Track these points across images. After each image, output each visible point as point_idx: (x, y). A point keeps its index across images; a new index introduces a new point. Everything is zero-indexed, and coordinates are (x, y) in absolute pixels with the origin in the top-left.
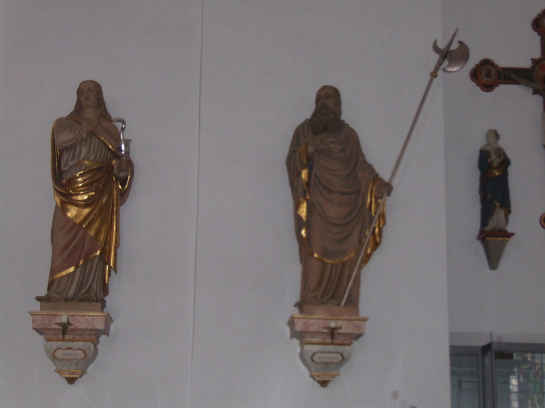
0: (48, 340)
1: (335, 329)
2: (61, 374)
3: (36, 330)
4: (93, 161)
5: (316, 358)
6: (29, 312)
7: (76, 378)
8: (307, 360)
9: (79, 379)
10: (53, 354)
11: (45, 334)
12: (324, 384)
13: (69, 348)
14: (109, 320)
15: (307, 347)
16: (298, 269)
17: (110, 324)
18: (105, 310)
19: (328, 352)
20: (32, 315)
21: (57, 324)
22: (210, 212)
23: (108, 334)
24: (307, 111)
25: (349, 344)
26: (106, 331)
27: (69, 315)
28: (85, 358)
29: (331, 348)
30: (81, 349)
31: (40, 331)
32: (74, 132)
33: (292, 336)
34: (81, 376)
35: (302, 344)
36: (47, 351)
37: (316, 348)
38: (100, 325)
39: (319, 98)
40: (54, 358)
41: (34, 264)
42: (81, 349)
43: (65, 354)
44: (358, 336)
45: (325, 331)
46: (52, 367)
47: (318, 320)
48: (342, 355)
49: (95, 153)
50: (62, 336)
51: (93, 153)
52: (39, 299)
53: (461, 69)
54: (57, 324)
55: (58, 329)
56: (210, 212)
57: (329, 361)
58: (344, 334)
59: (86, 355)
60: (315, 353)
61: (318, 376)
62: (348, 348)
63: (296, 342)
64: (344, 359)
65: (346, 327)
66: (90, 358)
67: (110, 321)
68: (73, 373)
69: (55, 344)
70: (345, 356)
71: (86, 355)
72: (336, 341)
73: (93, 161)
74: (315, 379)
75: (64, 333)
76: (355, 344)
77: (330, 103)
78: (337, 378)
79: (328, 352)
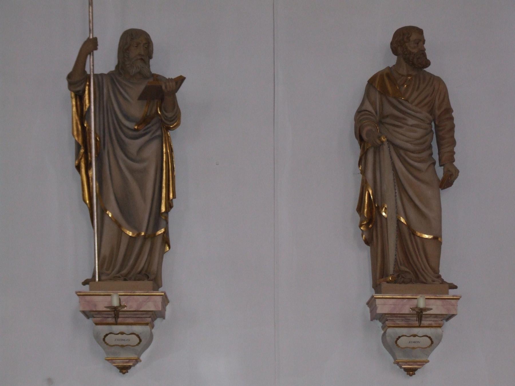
0: (97, 324)
3: (84, 312)
6: (76, 293)
7: (129, 367)
8: (392, 346)
9: (132, 368)
10: (104, 339)
13: (122, 333)
14: (165, 300)
15: (390, 331)
22: (264, 191)
23: (164, 317)
25: (440, 327)
27: (426, 299)
28: (139, 343)
30: (427, 336)
31: (87, 314)
32: (405, 119)
34: (134, 365)
36: (96, 336)
41: (66, 240)
42: (427, 336)
43: (119, 340)
44: (449, 317)
45: (108, 310)
49: (145, 132)
51: (145, 130)
53: (93, 55)
56: (264, 191)
58: (436, 316)
59: (140, 340)
60: (107, 335)
61: (406, 363)
62: (439, 330)
64: (433, 343)
65: (436, 307)
66: (143, 342)
69: (104, 329)
71: (140, 340)
72: (120, 320)
75: (420, 319)
78: (427, 365)
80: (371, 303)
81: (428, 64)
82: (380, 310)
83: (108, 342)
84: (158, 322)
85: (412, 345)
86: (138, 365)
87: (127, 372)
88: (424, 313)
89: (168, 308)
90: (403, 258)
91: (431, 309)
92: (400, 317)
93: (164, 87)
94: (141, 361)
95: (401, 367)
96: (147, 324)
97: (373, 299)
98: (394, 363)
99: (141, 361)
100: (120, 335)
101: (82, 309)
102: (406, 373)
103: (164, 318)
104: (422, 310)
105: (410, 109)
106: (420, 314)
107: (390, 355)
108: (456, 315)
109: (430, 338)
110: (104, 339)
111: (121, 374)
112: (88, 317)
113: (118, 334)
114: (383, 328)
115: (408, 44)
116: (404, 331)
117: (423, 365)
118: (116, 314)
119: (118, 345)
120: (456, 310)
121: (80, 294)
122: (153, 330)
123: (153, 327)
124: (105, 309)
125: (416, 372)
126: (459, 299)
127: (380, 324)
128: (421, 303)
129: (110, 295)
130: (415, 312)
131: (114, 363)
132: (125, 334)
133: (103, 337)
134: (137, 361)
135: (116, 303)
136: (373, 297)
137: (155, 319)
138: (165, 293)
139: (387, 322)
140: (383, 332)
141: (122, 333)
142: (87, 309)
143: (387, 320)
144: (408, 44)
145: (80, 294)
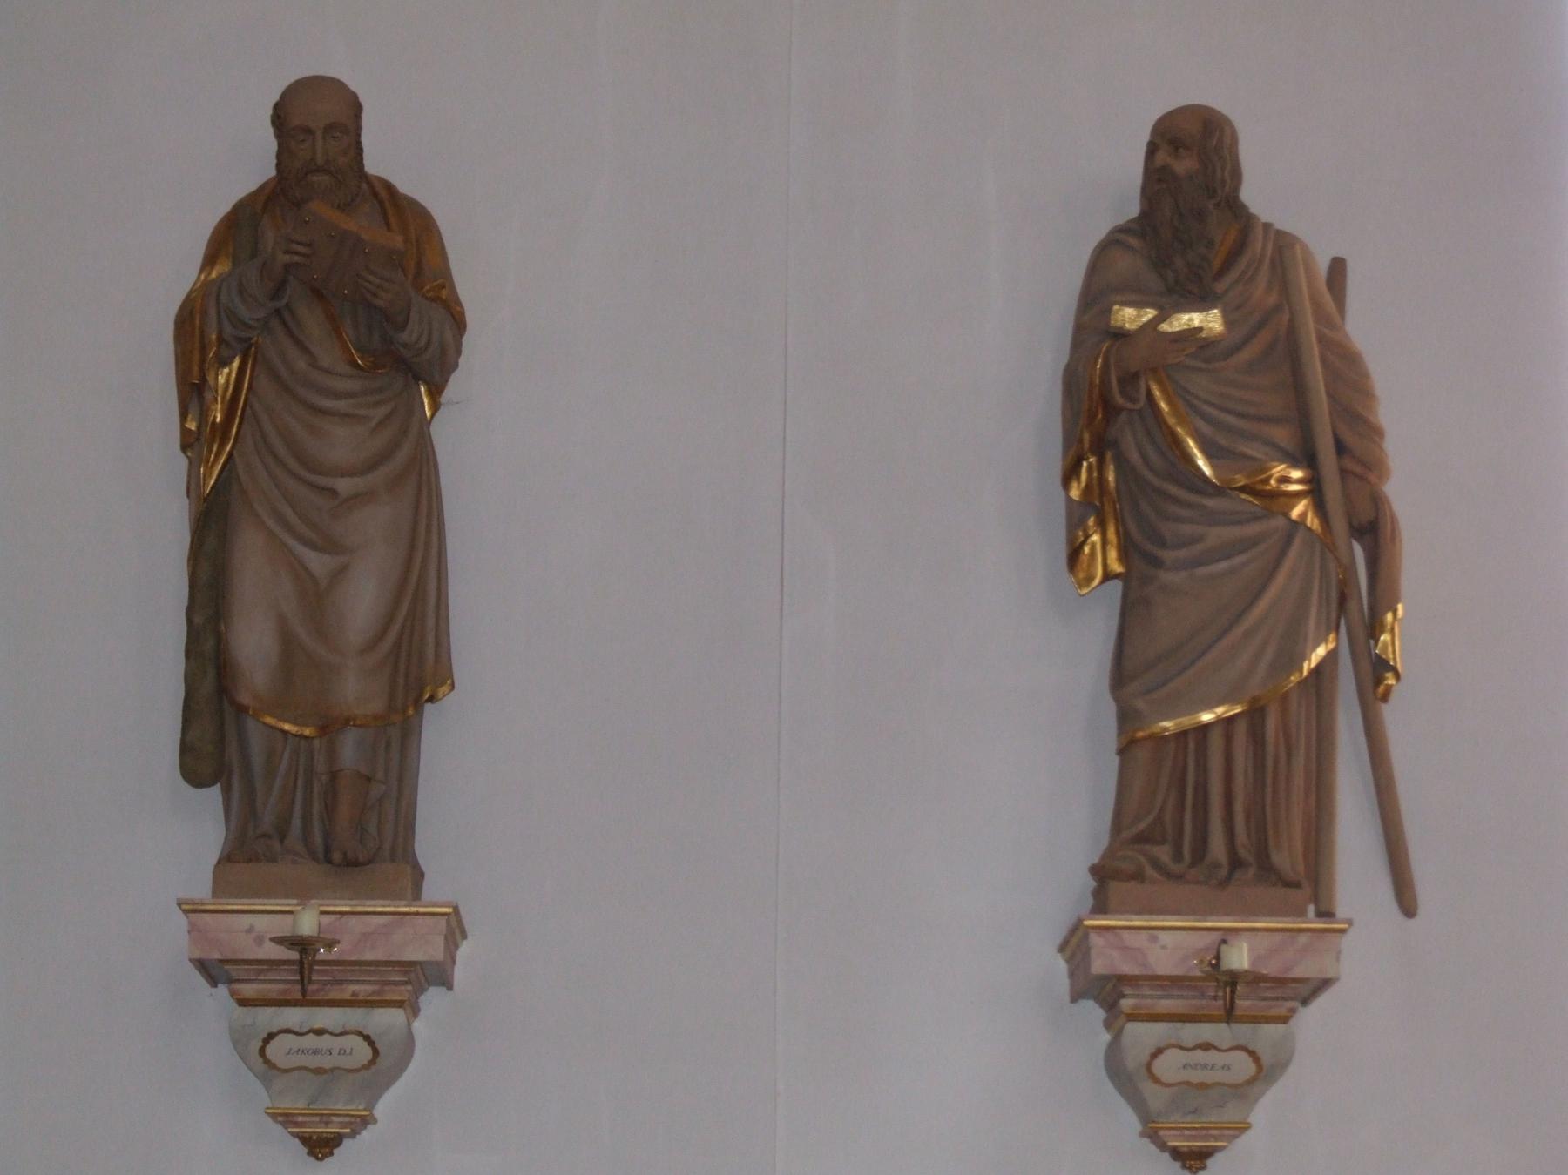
3: (202, 966)
5: (1160, 1066)
6: (179, 905)
9: (347, 1143)
10: (262, 1051)
11: (230, 981)
12: (320, 1147)
13: (1206, 1047)
15: (1134, 1030)
17: (457, 947)
18: (430, 890)
19: (319, 1032)
20: (185, 912)
21: (279, 941)
23: (448, 984)
24: (251, 162)
25: (1284, 1020)
26: (441, 976)
28: (373, 1062)
31: (212, 971)
33: (1076, 997)
34: (353, 1134)
35: (1115, 1018)
36: (238, 1040)
38: (431, 950)
39: (280, 117)
40: (269, 1069)
43: (1195, 1067)
50: (298, 987)
54: (279, 941)
57: (326, 1062)
59: (376, 1052)
63: (1092, 1012)
64: (1265, 1072)
66: (382, 1064)
67: (458, 936)
70: (1266, 1059)
71: (376, 1052)
74: (1162, 1146)
77: (1184, 165)
79: (319, 1032)
80: (1075, 945)
82: (1098, 966)
84: (433, 999)
85: (1196, 1076)
86: (366, 1135)
87: (1204, 1168)
89: (464, 950)
90: (1222, 813)
94: (375, 1121)
96: (399, 1004)
99: (375, 1121)
101: (197, 955)
102: (1178, 1165)
103: (450, 988)
108: (1325, 984)
109: (367, 1038)
110: (262, 1051)
111: (312, 1159)
112: (213, 981)
114: (1108, 1025)
115: (316, 127)
116: (293, 1016)
117: (1236, 1137)
118: (305, 972)
119: (306, 1068)
121: (191, 909)
122: (416, 1024)
123: (415, 1012)
125: (1210, 1162)
127: (1099, 1014)
128: (308, 923)
131: (297, 1124)
132: (1215, 1048)
133: (1145, 1057)
134: (365, 1121)
137: (423, 990)
138: (456, 909)
140: (1106, 1037)
144: (316, 127)
145: (191, 909)
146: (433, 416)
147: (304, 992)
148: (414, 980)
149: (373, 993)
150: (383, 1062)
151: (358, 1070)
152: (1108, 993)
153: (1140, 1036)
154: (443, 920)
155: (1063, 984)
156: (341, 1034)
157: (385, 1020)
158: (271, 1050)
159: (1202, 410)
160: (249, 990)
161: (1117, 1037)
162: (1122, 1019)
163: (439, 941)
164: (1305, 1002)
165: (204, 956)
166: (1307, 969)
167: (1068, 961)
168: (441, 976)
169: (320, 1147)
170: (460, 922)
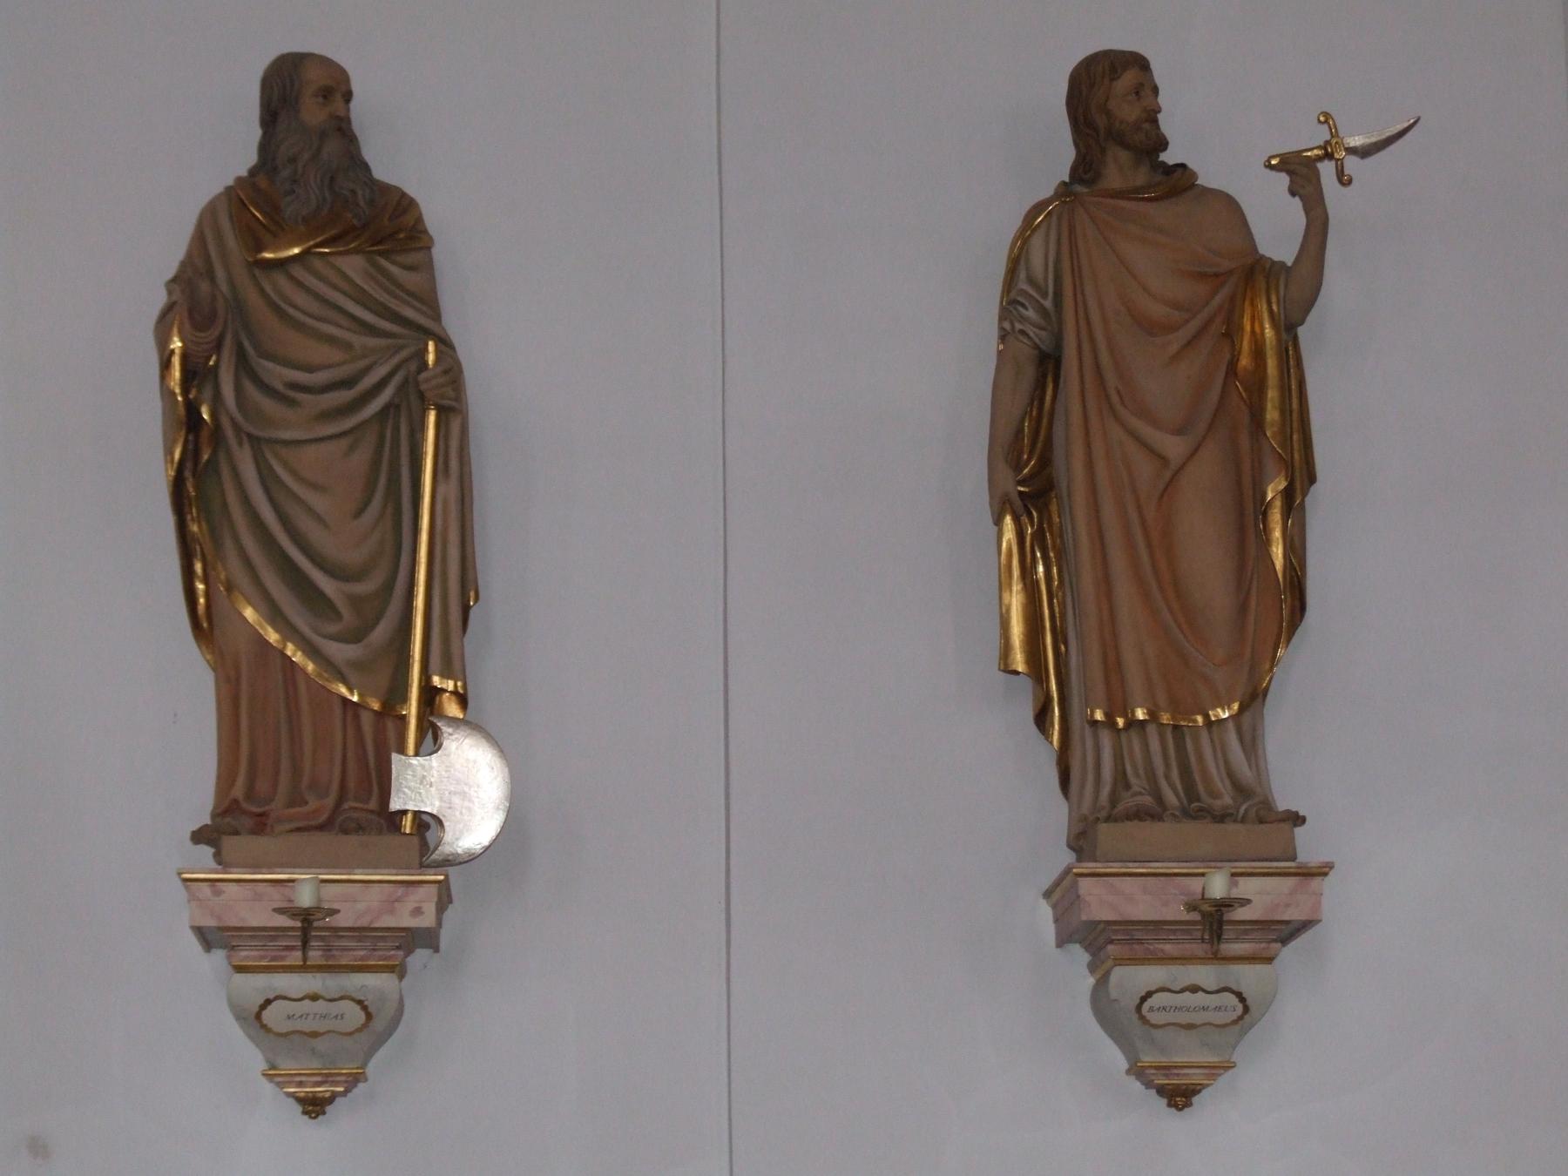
0: (240, 969)
1: (1225, 904)
2: (280, 1085)
3: (200, 932)
4: (307, 371)
6: (179, 874)
7: (331, 1099)
8: (1123, 1021)
10: (1139, 1008)
15: (1119, 974)
16: (257, 133)
21: (280, 911)
25: (1269, 960)
27: (1233, 875)
28: (365, 1026)
29: (1205, 974)
31: (207, 938)
33: (1061, 942)
34: (344, 1094)
37: (1152, 975)
46: (252, 1058)
47: (258, 893)
48: (1241, 997)
50: (299, 954)
52: (199, 837)
55: (292, 929)
57: (1197, 1018)
59: (1246, 1009)
65: (1261, 895)
66: (377, 1025)
68: (327, 1079)
69: (256, 986)
71: (369, 1016)
73: (307, 371)
76: (1289, 954)
80: (1062, 894)
81: (1163, 144)
83: (270, 1025)
88: (316, 924)
91: (337, 911)
92: (1174, 931)
93: (355, 222)
95: (1148, 1084)
96: (390, 969)
97: (1069, 878)
98: (1128, 1072)
100: (307, 1002)
104: (307, 917)
105: (295, 307)
106: (1214, 921)
107: (1109, 1042)
113: (1182, 991)
114: (1092, 968)
115: (303, 102)
120: (1317, 906)
124: (283, 921)
125: (1195, 1099)
126: (1326, 874)
128: (1218, 886)
129: (1203, 875)
130: (1196, 916)
135: (305, 898)
136: (1068, 871)
139: (1110, 947)
140: (1091, 981)
141: (1194, 989)
142: (210, 922)
143: (1112, 942)
144: (303, 102)
146: (1022, 422)
147: (305, 959)
148: (1288, 931)
149: (362, 959)
150: (379, 1024)
151: (351, 1034)
152: (1104, 942)
153: (1132, 979)
154: (434, 889)
155: (1049, 930)
156: (1217, 992)
157: (1247, 977)
158: (266, 1014)
159: (1150, 404)
160: (245, 956)
161: (1102, 983)
162: (1110, 963)
163: (430, 909)
164: (1284, 941)
165: (202, 924)
166: (1294, 915)
167: (1054, 907)
168: (428, 939)
169: (1180, 1096)
170: (448, 889)
